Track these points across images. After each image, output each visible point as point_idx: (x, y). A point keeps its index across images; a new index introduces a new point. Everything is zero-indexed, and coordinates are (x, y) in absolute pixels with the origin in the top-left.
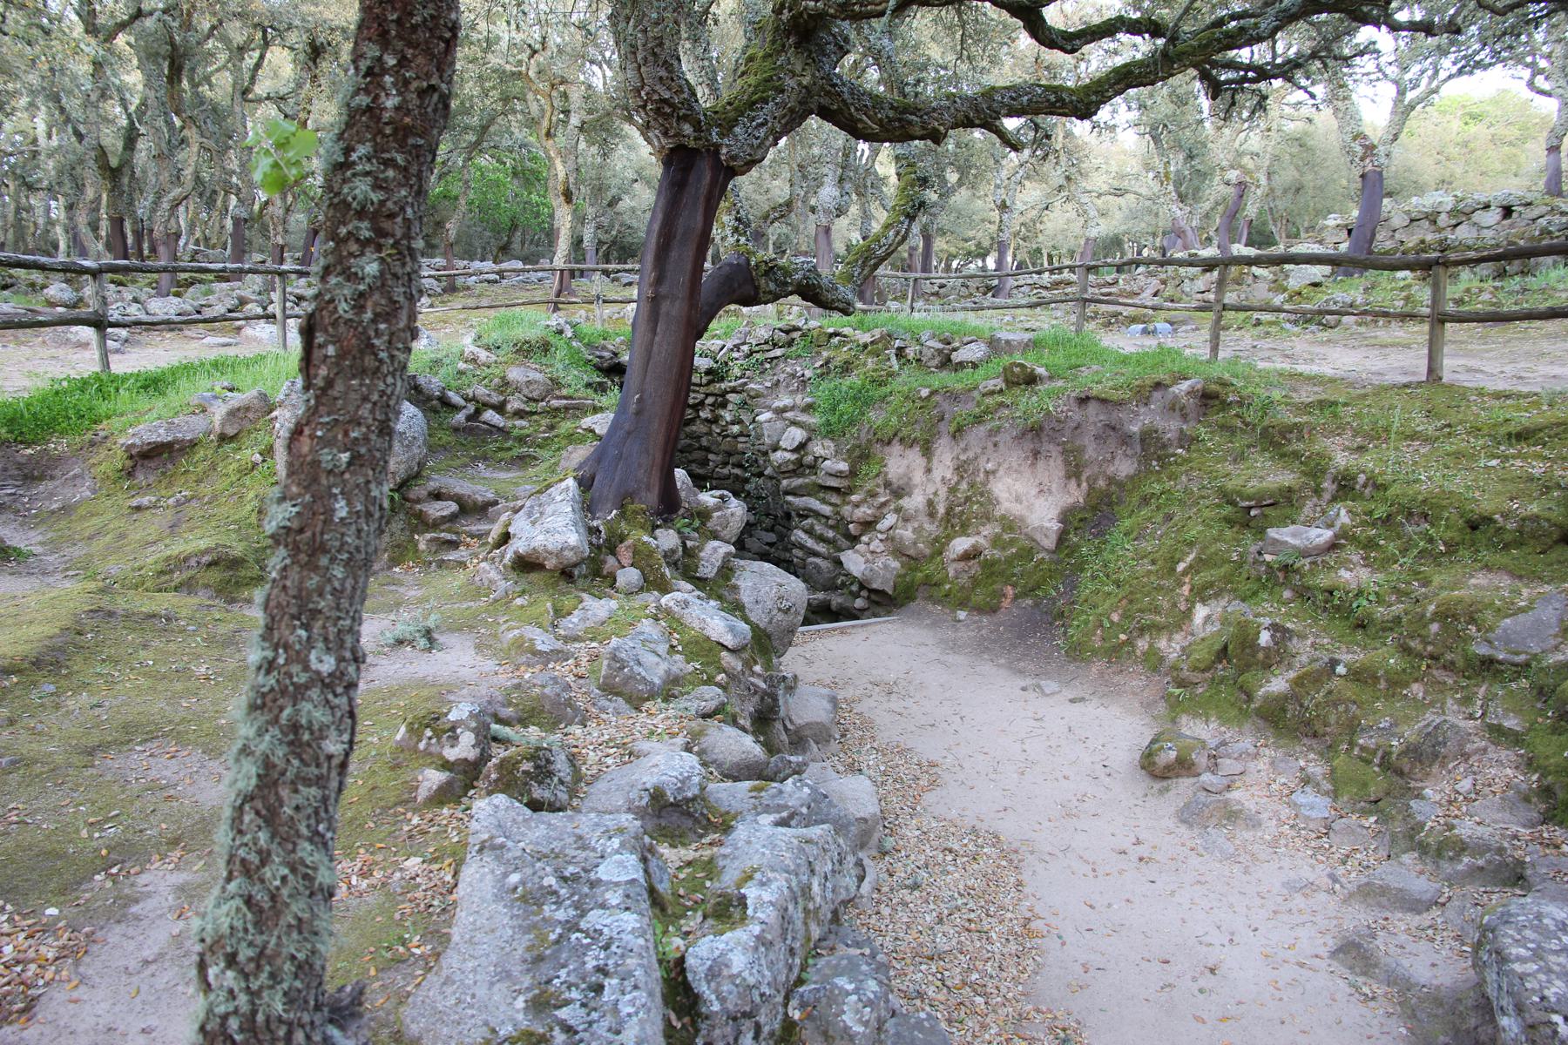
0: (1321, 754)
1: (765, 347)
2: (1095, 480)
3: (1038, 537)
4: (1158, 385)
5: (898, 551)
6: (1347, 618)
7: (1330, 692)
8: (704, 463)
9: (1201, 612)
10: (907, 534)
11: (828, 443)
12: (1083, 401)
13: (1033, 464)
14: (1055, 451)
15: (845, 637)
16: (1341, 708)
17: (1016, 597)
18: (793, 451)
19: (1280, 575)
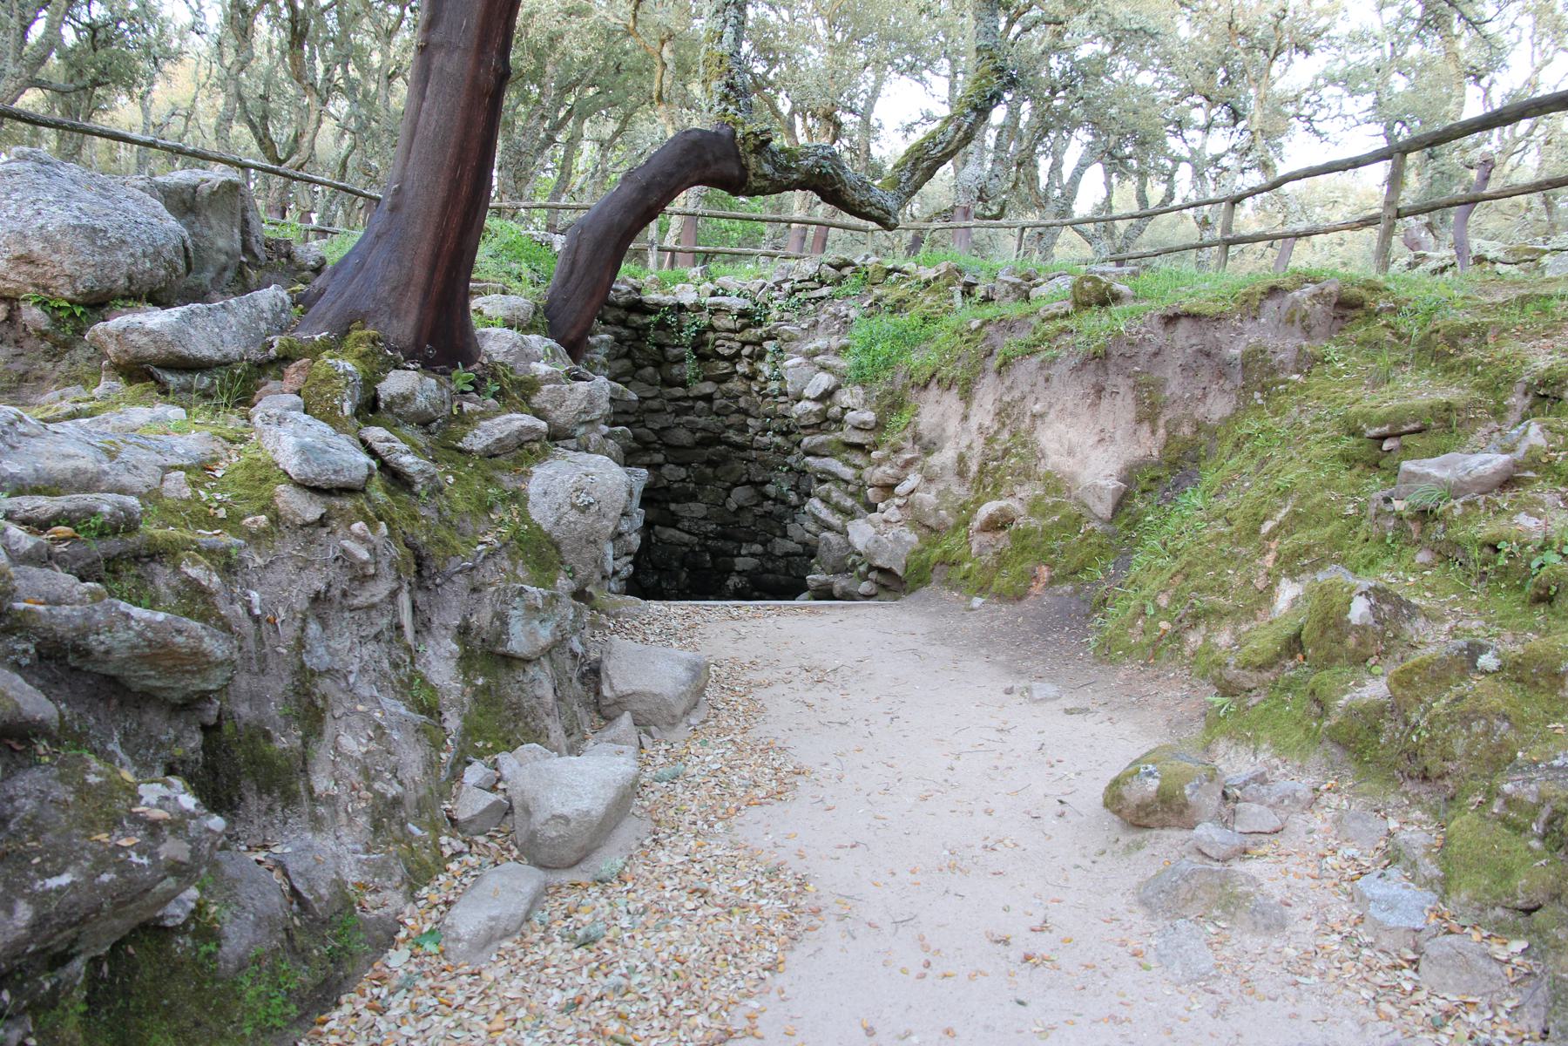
0: (1434, 812)
1: (810, 285)
2: (1178, 425)
3: (1090, 501)
4: (1273, 291)
5: (918, 523)
6: (1521, 588)
7: (1460, 698)
8: (743, 429)
9: (1287, 592)
10: (928, 498)
11: (858, 390)
12: (1171, 320)
13: (1093, 405)
14: (1123, 385)
15: (813, 617)
16: (1478, 727)
17: (1052, 581)
18: (816, 400)
19: (1413, 527)
